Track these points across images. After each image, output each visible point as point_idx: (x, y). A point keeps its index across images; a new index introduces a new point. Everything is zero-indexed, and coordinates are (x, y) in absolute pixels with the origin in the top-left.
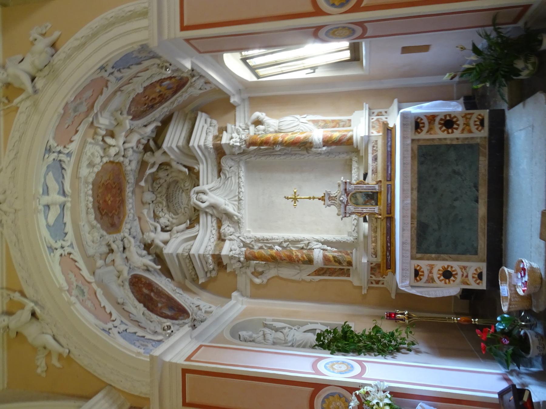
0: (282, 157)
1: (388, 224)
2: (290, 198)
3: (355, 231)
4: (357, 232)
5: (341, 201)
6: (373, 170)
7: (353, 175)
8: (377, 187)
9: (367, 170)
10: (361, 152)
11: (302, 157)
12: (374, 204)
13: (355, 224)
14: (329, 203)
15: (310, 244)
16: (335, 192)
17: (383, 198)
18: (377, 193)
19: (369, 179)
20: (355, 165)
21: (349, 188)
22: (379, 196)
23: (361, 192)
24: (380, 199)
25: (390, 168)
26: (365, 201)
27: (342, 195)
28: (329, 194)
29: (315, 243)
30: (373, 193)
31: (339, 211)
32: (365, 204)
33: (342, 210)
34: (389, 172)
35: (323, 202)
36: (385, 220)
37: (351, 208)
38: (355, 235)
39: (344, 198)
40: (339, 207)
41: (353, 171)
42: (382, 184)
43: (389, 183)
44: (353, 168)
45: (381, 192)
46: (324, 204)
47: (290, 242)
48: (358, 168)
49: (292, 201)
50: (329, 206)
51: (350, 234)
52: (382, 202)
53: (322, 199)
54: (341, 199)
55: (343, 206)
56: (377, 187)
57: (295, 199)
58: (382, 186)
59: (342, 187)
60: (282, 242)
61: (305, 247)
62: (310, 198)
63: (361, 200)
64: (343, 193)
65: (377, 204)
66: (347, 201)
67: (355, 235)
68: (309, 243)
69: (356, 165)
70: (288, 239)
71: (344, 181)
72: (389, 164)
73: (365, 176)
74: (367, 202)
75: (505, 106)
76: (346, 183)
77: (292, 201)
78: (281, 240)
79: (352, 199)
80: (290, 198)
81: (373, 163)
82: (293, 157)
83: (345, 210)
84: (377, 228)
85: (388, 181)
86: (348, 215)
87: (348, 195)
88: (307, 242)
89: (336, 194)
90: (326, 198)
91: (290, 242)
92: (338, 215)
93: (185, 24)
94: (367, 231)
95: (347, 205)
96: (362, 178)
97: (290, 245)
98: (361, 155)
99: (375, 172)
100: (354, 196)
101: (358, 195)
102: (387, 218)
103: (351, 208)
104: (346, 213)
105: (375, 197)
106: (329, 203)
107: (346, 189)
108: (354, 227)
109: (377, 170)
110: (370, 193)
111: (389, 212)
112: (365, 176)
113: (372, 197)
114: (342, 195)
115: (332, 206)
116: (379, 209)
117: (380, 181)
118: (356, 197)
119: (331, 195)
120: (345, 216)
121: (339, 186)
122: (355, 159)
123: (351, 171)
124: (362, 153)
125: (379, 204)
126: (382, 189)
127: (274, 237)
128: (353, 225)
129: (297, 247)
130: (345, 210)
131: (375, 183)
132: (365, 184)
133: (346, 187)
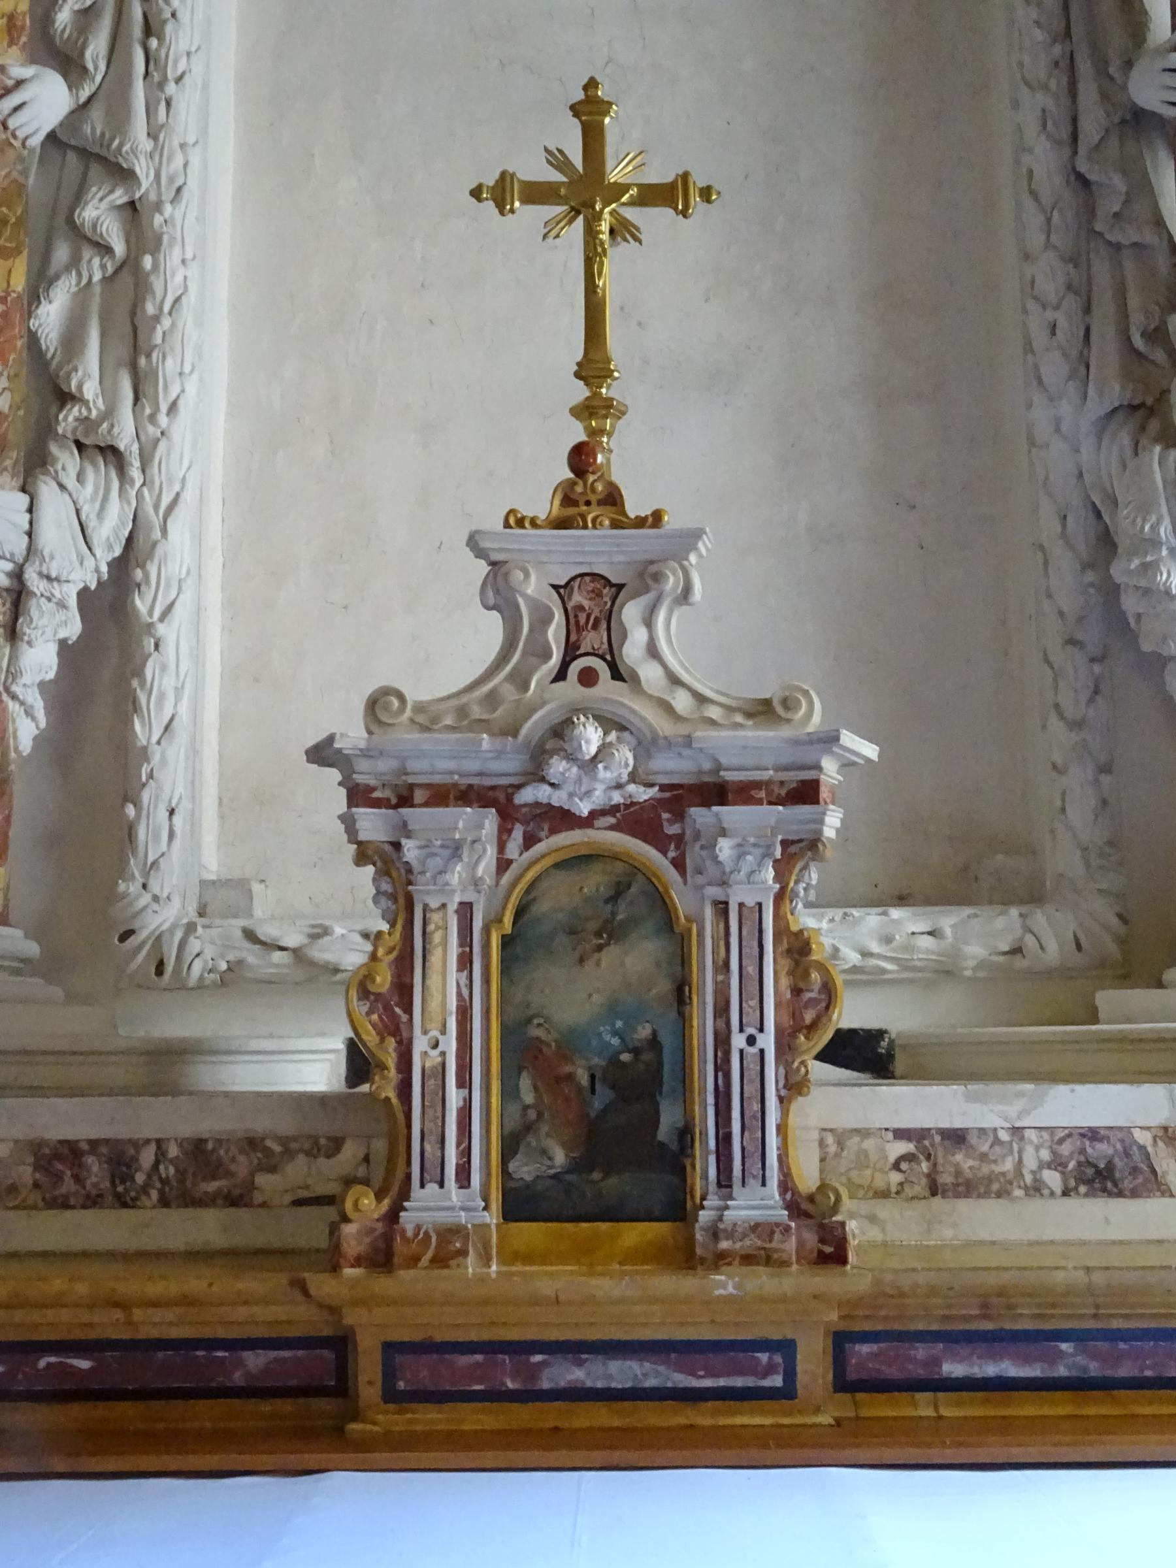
0: (1045, 159)
1: (255, 1360)
2: (593, 137)
3: (251, 955)
4: (231, 979)
5: (561, 732)
6: (956, 1137)
7: (871, 920)
8: (754, 1204)
9: (923, 1074)
10: (1140, 997)
11: (1055, 368)
12: (524, 1169)
13: (324, 953)
14: (534, 587)
15: (98, 474)
16: (697, 649)
17: (609, 1286)
18: (679, 1210)
19: (840, 1102)
20: (977, 935)
21: (737, 841)
22: (634, 1234)
23: (681, 994)
24: (585, 1254)
25: (1010, 1369)
26: (570, 1044)
27: (646, 746)
28: (647, 577)
29: (110, 531)
30: (675, 1159)
31: (427, 718)
32: (524, 1050)
33: (439, 757)
34: (953, 1369)
35: (540, 503)
36: (300, 1317)
37: (468, 865)
38: (207, 952)
39: (599, 774)
40: (463, 713)
41: (907, 921)
42: (796, 1281)
43: (814, 1365)
44: (949, 920)
45: (686, 1257)
46: (516, 521)
47: (130, 264)
48: (946, 971)
49: (558, 160)
50: (498, 590)
51: (220, 898)
52: (554, 1280)
53: (586, 493)
54: (591, 737)
55: (493, 758)
56: (754, 1204)
57: (582, 191)
58: (762, 1280)
59: (744, 749)
60: (126, 176)
61: (68, 419)
62: (593, 367)
63: (578, 997)
64: (674, 767)
65: (519, 1205)
66: (563, 819)
67: (207, 952)
68: (112, 454)
69: (975, 951)
70: (155, 246)
71: (830, 770)
72: (1069, 1360)
73: (864, 1054)
74: (554, 1081)
75: (529, 829)
76: (806, 793)
77: (558, 160)
78: (142, 168)
79: (595, 881)
80: (593, 137)
81: (1056, 1136)
82: (1049, 275)
83: (443, 795)
84: (235, 1200)
85: (841, 1341)
86: (373, 824)
87: (635, 820)
88: (125, 435)
89: (650, 674)
90: (599, 548)
91: (130, 264)
92: (378, 706)
93: (399, 1359)
94: (247, 1076)
95: (508, 814)
96: (853, 1013)
97: (96, 268)
98: (1107, 999)
99: (940, 1166)
100: (631, 906)
101: (637, 959)
102: (341, 1344)
103: (468, 865)
104: (405, 800)
105: (614, 1185)
106: (534, 587)
107: (717, 793)
108: (293, 939)
109: (967, 1188)
110: (669, 1118)
111: (417, 1373)
112: (864, 1054)
113: (620, 1138)
114: (646, 746)
115: (492, 627)
116: (448, 1245)
117: (832, 1252)
118: (612, 932)
119: (631, 612)
120: (358, 795)
121: (763, 711)
122: (1051, 934)
123: (902, 900)
124: (1128, 1010)
125: (531, 1232)
126: (724, 1283)
127: (186, 101)
128: (320, 933)
129: (72, 339)
130: (443, 795)
131: (807, 1178)
132: (785, 1046)
133: (744, 793)
